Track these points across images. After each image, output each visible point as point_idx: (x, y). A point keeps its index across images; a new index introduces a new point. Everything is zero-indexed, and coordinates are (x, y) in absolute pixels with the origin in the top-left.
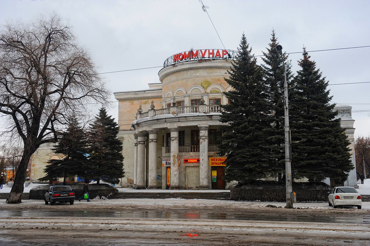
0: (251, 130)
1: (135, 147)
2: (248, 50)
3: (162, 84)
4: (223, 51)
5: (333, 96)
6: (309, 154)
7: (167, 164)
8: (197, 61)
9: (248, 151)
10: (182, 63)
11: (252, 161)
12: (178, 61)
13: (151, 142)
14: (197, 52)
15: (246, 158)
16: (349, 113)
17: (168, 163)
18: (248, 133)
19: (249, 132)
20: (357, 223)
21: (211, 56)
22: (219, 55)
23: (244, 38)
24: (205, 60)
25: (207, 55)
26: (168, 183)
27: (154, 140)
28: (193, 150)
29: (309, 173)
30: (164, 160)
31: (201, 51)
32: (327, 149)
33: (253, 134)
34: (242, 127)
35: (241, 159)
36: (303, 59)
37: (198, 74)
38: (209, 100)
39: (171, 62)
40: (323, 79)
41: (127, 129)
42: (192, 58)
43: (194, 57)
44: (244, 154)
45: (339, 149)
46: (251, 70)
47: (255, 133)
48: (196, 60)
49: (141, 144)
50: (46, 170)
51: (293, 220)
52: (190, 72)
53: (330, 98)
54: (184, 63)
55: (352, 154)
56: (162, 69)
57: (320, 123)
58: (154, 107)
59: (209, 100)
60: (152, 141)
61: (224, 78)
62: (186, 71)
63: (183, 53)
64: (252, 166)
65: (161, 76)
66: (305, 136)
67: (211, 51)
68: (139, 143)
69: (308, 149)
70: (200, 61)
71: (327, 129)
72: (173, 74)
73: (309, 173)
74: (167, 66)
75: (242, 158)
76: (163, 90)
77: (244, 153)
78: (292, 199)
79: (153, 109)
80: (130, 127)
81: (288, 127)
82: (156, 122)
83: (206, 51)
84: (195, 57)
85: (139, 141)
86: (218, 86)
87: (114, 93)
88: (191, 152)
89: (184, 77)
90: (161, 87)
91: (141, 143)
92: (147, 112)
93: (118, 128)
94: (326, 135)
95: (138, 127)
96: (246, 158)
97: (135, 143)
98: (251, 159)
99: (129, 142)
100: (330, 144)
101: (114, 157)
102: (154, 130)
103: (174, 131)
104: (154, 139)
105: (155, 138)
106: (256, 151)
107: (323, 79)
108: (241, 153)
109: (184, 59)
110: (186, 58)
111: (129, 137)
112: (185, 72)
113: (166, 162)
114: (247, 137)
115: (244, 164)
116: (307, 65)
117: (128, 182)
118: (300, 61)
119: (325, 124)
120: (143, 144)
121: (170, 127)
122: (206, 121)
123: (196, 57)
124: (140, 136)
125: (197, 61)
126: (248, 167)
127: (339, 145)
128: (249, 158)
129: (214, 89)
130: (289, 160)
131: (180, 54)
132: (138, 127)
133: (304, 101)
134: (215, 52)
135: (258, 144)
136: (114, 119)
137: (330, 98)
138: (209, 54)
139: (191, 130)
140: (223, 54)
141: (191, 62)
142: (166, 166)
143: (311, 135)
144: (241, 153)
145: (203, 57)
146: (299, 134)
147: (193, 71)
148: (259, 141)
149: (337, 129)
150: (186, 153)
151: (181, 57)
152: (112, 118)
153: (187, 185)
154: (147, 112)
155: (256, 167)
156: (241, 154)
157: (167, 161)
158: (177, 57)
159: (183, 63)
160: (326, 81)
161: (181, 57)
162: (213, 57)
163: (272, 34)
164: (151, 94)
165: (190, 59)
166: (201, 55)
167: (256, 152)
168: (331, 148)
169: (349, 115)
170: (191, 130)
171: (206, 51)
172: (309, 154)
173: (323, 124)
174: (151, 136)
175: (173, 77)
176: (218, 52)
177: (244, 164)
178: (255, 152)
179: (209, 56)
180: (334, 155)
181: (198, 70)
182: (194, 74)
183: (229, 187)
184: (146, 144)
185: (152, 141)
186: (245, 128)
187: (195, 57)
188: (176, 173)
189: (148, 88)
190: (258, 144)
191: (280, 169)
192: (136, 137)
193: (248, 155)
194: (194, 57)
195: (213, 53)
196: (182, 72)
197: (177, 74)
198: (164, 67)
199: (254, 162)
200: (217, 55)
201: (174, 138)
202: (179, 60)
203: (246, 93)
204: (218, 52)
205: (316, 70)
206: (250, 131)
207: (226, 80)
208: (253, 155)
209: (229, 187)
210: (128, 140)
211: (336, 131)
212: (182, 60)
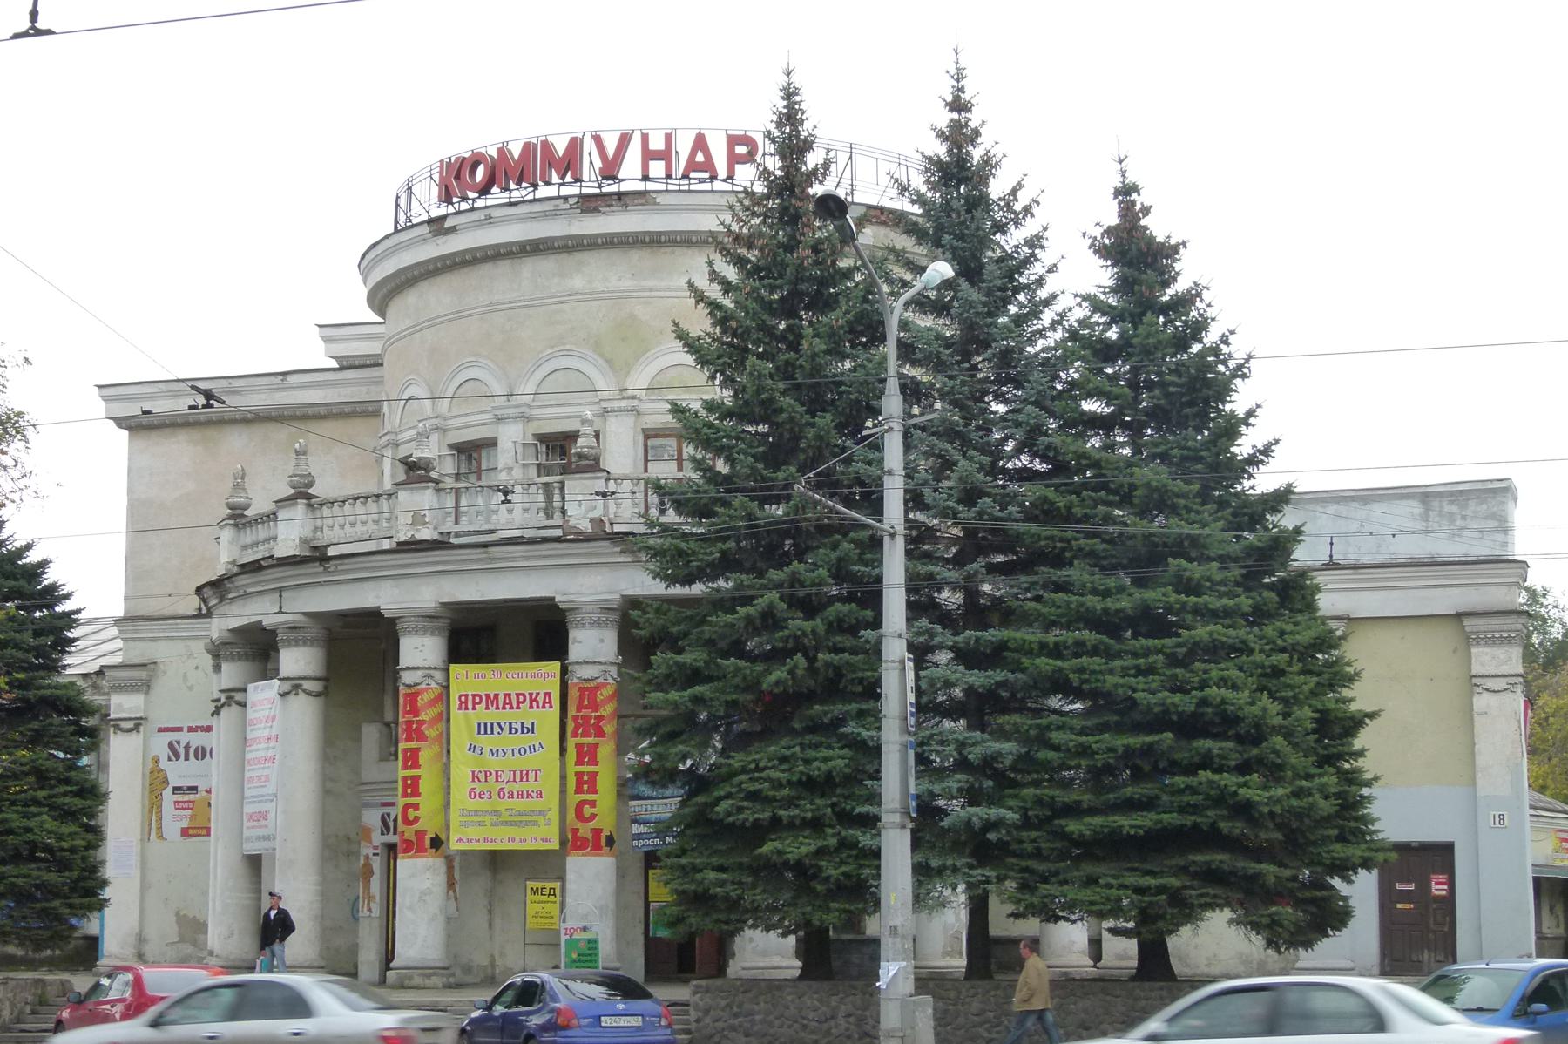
0: (796, 637)
2: (813, 160)
3: (380, 329)
4: (733, 141)
5: (1277, 442)
6: (1099, 775)
7: (386, 828)
8: (572, 201)
9: (784, 759)
10: (481, 215)
11: (804, 819)
12: (465, 199)
14: (575, 145)
15: (768, 800)
16: (1493, 516)
18: (777, 656)
19: (790, 646)
21: (657, 169)
22: (708, 166)
23: (789, 94)
24: (620, 196)
25: (631, 167)
27: (307, 685)
29: (1110, 886)
31: (598, 140)
32: (1210, 750)
33: (811, 660)
34: (749, 620)
35: (740, 810)
36: (1113, 220)
37: (578, 283)
38: (641, 438)
39: (427, 202)
40: (1224, 340)
41: (182, 611)
42: (548, 183)
43: (555, 179)
44: (757, 779)
45: (1276, 752)
46: (823, 283)
47: (820, 655)
48: (566, 198)
52: (530, 268)
53: (1262, 452)
54: (496, 213)
55: (1376, 779)
56: (374, 245)
57: (1177, 601)
58: (310, 485)
59: (647, 438)
61: (676, 325)
63: (493, 152)
64: (799, 847)
65: (372, 281)
66: (1093, 672)
67: (657, 144)
68: (229, 698)
69: (1103, 746)
70: (590, 204)
71: (1215, 636)
73: (1110, 886)
74: (406, 228)
75: (745, 804)
76: (385, 371)
77: (757, 769)
78: (909, 1031)
79: (309, 497)
80: (193, 604)
81: (900, 636)
82: (316, 574)
83: (625, 140)
84: (563, 178)
86: (633, 370)
87: (100, 387)
89: (497, 298)
90: (373, 348)
92: (272, 517)
93: (69, 619)
94: (1205, 672)
95: (222, 599)
96: (768, 800)
98: (797, 806)
99: (190, 688)
100: (1226, 723)
101: (42, 788)
102: (302, 618)
103: (416, 631)
104: (304, 678)
106: (825, 760)
107: (1224, 340)
108: (744, 770)
109: (495, 190)
110: (507, 183)
112: (504, 266)
114: (773, 677)
115: (759, 833)
116: (1136, 254)
117: (180, 935)
118: (1098, 232)
119: (1206, 605)
122: (604, 570)
123: (568, 178)
125: (572, 201)
126: (780, 852)
127: (1276, 730)
128: (790, 802)
129: (673, 372)
130: (897, 818)
131: (476, 161)
132: (222, 599)
133: (1100, 468)
134: (683, 147)
135: (840, 721)
136: (44, 564)
137: (1262, 452)
138: (648, 155)
140: (733, 160)
141: (537, 207)
143: (1123, 668)
144: (744, 770)
145: (610, 172)
146: (1059, 663)
147: (547, 264)
148: (845, 701)
149: (1282, 633)
151: (480, 173)
152: (33, 557)
153: (502, 954)
154: (272, 517)
155: (821, 852)
156: (743, 777)
158: (458, 176)
159: (487, 212)
160: (1237, 350)
161: (480, 173)
162: (669, 176)
163: (953, 71)
165: (535, 186)
166: (598, 164)
167: (824, 767)
168: (1231, 745)
169: (1495, 530)
171: (625, 140)
172: (1099, 775)
173: (1195, 604)
175: (434, 297)
176: (700, 143)
177: (759, 833)
178: (818, 769)
179: (645, 168)
180: (1245, 785)
182: (556, 280)
186: (769, 620)
187: (563, 178)
188: (427, 884)
189: (317, 356)
190: (840, 721)
191: (954, 866)
192: (218, 653)
193: (778, 785)
194: (555, 179)
195: (666, 155)
196: (486, 269)
198: (396, 231)
199: (816, 825)
200: (692, 166)
201: (420, 673)
202: (471, 195)
203: (785, 415)
204: (700, 143)
205: (1180, 286)
206: (797, 645)
207: (682, 336)
208: (810, 785)
210: (185, 677)
211: (1274, 643)
212: (484, 191)
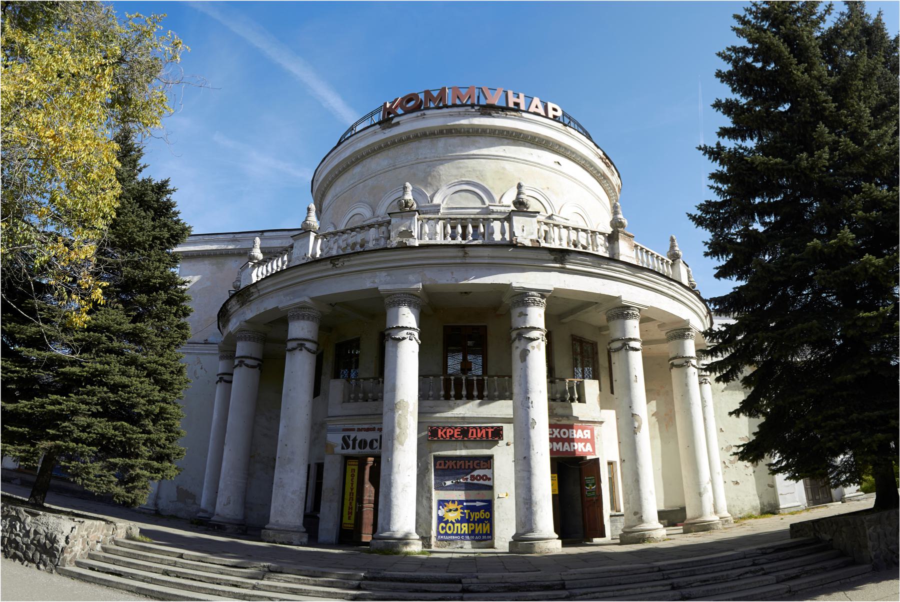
1: (219, 388)
13: (297, 352)
17: (355, 440)
26: (346, 520)
49: (247, 366)
50: (513, 537)
51: (554, 585)
60: (302, 345)
72: (379, 155)
85: (243, 354)
88: (456, 399)
91: (248, 361)
95: (243, 304)
97: (220, 372)
113: (344, 439)
121: (388, 287)
124: (245, 339)
142: (345, 452)
150: (439, 402)
157: (347, 433)
164: (280, 241)
170: (445, 327)
181: (473, 138)
183: (625, 532)
184: (270, 368)
185: (302, 345)
196: (414, 145)
197: (392, 153)
209: (625, 532)
210: (195, 372)
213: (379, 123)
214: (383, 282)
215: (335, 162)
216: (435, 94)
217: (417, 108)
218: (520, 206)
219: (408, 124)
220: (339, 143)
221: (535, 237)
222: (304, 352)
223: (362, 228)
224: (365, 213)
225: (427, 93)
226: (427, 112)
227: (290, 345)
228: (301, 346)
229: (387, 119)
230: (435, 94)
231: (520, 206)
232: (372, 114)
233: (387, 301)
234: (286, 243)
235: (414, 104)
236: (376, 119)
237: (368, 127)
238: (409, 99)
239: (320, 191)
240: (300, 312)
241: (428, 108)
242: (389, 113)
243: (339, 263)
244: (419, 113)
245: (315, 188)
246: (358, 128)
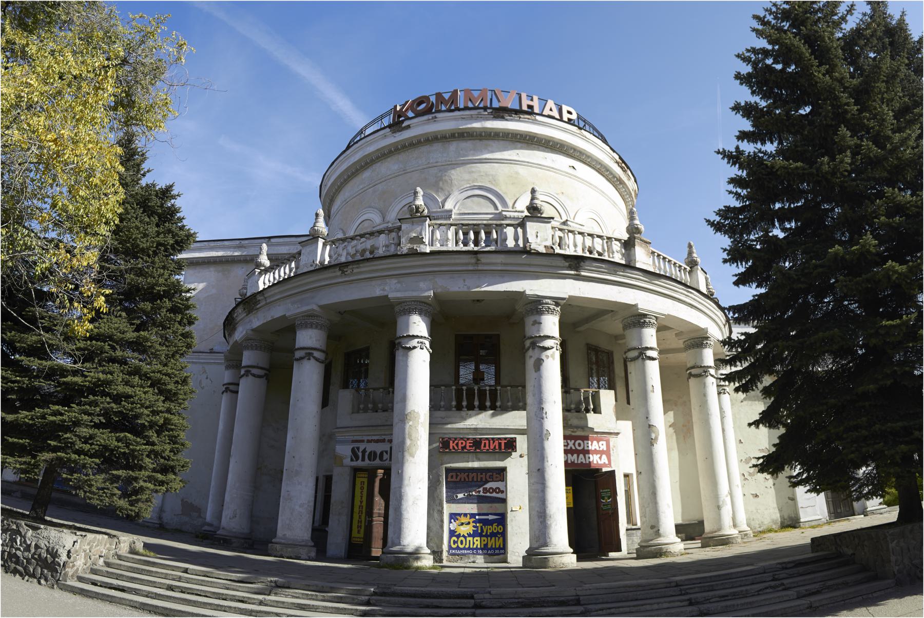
1: (225, 399)
13: (305, 362)
17: (364, 451)
20: (436, 515)
28: (464, 403)
30: (342, 442)
49: (254, 375)
62: (440, 144)
85: (249, 363)
88: (469, 409)
91: (254, 371)
105: (318, 346)
111: (205, 372)
112: (437, 146)
113: (353, 450)
120: (259, 377)
121: (399, 295)
124: (251, 348)
139: (457, 336)
142: (354, 464)
157: (356, 445)
164: (287, 248)
170: (457, 336)
174: (308, 338)
181: (485, 142)
183: (641, 546)
184: (277, 378)
196: (424, 149)
197: (402, 157)
209: (641, 546)
213: (390, 126)
214: (393, 290)
215: (344, 166)
216: (447, 96)
217: (428, 111)
218: (534, 212)
219: (419, 128)
220: (348, 147)
221: (549, 243)
222: (312, 361)
223: (372, 234)
224: (375, 219)
225: (439, 96)
226: (438, 115)
227: (298, 354)
228: (309, 356)
229: (398, 122)
230: (447, 96)
231: (534, 212)
232: (382, 117)
233: (397, 309)
234: (294, 249)
235: (425, 107)
236: (386, 122)
237: (378, 131)
238: (420, 101)
239: (329, 196)
240: (308, 320)
241: (440, 111)
242: (399, 116)
243: (348, 270)
244: (430, 116)
245: (324, 193)
246: (368, 132)
